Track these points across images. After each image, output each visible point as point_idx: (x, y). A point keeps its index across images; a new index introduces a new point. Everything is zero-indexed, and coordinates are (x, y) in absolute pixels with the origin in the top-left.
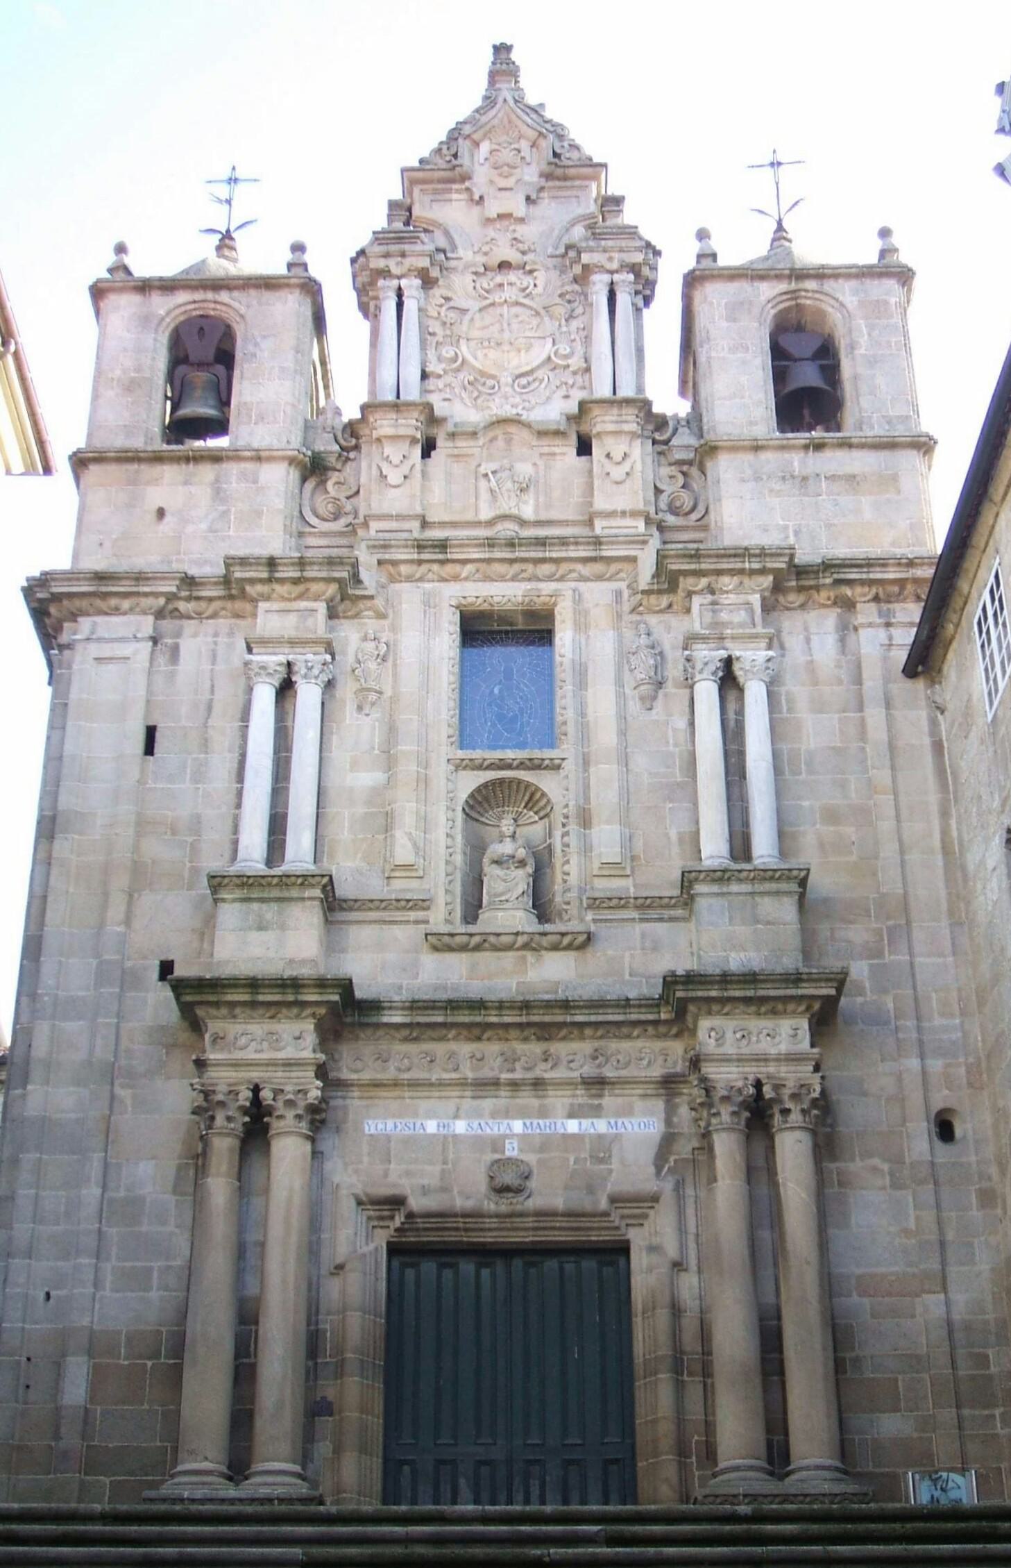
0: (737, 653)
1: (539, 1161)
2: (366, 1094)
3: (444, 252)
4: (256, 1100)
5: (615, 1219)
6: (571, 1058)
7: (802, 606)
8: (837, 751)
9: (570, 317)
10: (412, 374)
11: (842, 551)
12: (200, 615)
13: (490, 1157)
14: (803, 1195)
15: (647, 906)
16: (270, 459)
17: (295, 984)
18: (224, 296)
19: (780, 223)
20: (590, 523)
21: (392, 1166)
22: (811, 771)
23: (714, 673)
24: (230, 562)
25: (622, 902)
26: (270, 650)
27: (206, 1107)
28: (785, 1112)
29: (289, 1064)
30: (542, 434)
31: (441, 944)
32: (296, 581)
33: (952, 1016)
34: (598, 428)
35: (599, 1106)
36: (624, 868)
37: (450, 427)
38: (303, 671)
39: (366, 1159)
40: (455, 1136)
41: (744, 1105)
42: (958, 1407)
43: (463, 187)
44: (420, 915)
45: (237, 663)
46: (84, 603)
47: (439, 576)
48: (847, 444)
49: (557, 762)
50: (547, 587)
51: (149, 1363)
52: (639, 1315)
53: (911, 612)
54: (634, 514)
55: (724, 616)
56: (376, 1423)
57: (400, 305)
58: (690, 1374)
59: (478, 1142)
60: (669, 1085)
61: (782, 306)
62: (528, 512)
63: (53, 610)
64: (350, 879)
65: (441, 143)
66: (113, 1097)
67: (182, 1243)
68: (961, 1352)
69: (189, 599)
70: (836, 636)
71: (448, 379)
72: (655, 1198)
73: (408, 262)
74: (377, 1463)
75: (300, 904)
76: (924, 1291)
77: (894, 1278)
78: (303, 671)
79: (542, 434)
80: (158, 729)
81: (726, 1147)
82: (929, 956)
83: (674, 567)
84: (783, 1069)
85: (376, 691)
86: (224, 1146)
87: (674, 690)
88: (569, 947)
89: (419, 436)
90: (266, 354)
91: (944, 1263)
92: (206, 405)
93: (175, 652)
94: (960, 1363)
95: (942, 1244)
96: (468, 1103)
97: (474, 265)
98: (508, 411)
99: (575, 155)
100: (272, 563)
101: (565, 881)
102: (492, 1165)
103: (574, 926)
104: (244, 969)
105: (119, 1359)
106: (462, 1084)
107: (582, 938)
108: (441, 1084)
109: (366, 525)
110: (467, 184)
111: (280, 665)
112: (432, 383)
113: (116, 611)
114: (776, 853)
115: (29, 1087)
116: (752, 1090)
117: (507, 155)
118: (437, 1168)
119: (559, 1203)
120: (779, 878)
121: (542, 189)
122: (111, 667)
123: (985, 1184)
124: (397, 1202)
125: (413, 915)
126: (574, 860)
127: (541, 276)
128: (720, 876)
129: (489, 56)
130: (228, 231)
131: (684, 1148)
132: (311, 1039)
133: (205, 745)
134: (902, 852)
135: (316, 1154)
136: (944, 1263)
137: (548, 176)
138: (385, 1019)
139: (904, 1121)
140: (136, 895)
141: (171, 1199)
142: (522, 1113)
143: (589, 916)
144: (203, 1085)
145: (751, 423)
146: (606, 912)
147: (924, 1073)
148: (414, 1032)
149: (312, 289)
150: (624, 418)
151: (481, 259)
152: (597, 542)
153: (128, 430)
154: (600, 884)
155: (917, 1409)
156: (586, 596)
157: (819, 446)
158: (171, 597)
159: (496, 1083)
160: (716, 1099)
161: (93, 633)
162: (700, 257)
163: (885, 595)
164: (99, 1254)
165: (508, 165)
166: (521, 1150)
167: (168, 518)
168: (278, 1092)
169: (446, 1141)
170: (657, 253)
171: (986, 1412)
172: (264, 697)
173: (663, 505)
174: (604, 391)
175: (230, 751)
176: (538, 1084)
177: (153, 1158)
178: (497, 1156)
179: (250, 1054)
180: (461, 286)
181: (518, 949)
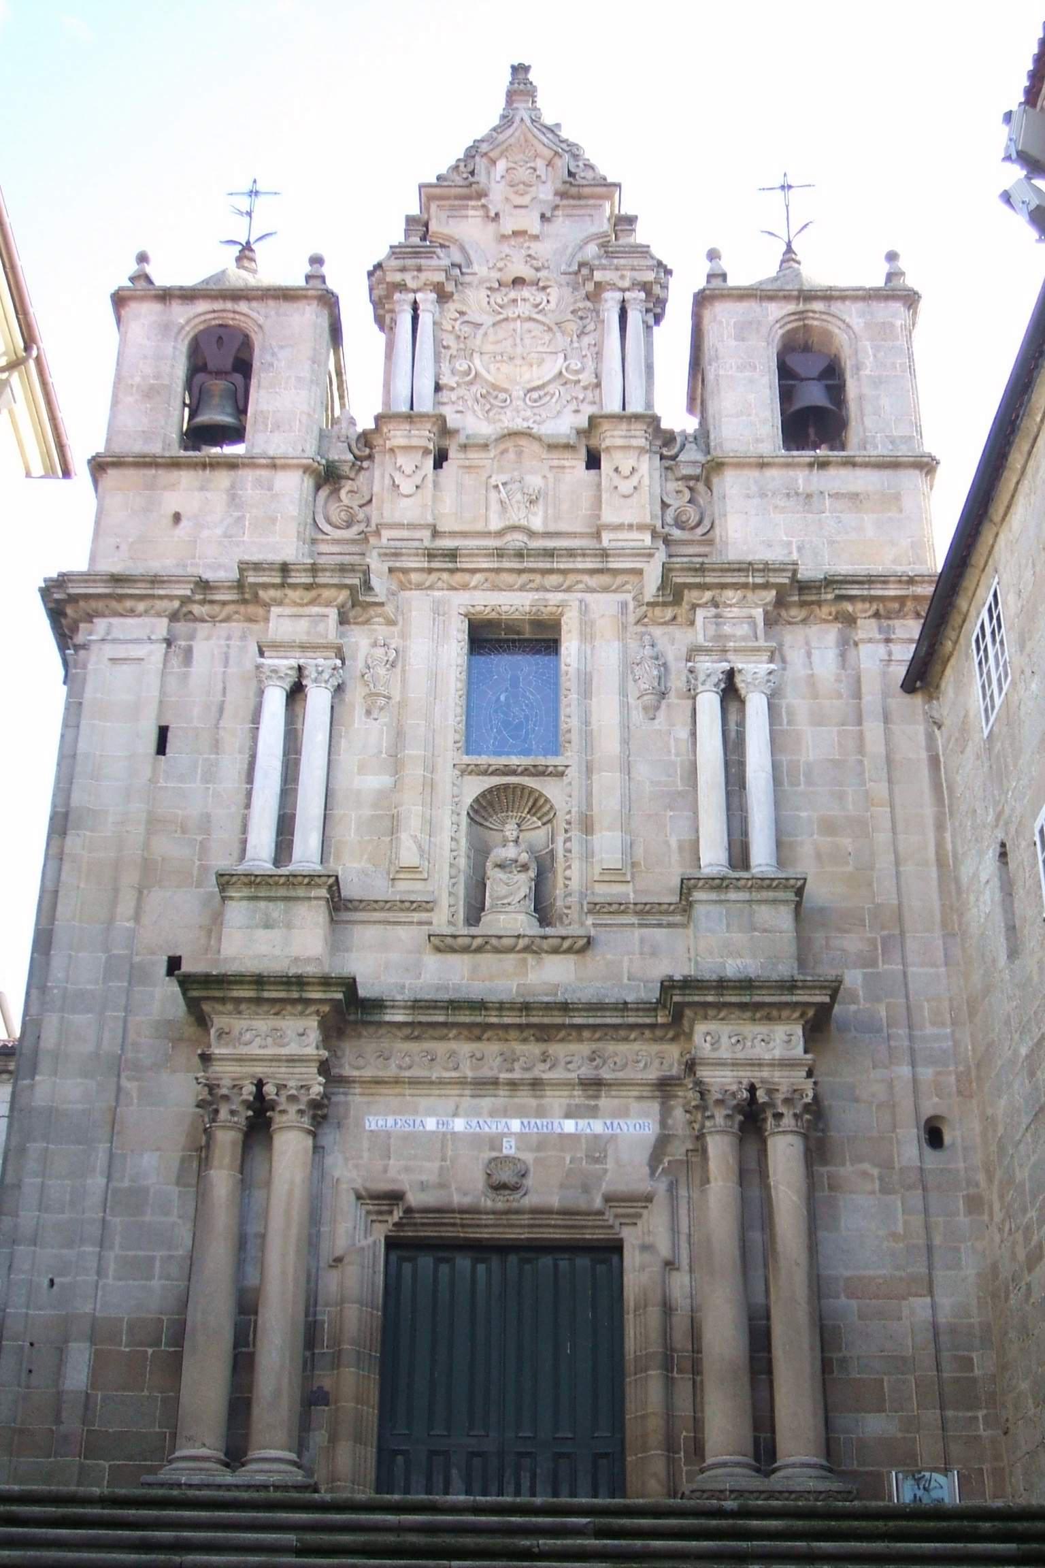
1: (536, 1160)
2: (367, 1091)
3: (460, 267)
4: (260, 1094)
5: (609, 1217)
6: (569, 1059)
7: (804, 621)
8: (837, 764)
9: (582, 334)
10: (425, 386)
11: (843, 568)
12: (213, 618)
13: (488, 1155)
14: (795, 1198)
15: (647, 912)
16: (285, 467)
17: (299, 982)
18: (243, 307)
19: (789, 244)
20: (597, 535)
21: (392, 1162)
22: (809, 783)
23: (716, 685)
24: (244, 567)
25: (622, 907)
27: (210, 1101)
29: (292, 1060)
30: (552, 447)
31: (444, 945)
32: (308, 587)
33: (943, 1024)
34: (607, 443)
36: (625, 874)
37: (462, 439)
38: (314, 675)
39: (366, 1155)
40: (454, 1134)
41: (738, 1108)
42: (942, 1408)
43: (480, 203)
44: (424, 916)
45: (249, 666)
46: (100, 605)
48: (850, 463)
49: (560, 769)
50: (555, 598)
51: (150, 1351)
52: (631, 1312)
53: (910, 628)
54: (641, 527)
55: (727, 629)
56: (371, 1413)
57: (415, 319)
58: (680, 1371)
59: (476, 1140)
60: (664, 1087)
61: (789, 326)
62: (537, 524)
63: (69, 611)
64: (355, 880)
65: (459, 160)
67: (184, 1234)
68: (945, 1355)
69: (203, 602)
70: (837, 651)
71: (461, 391)
72: (649, 1199)
73: (424, 276)
74: (371, 1452)
75: (306, 904)
76: (910, 1294)
77: (881, 1281)
79: (552, 447)
80: (170, 729)
81: (720, 1149)
83: (679, 580)
84: (777, 1074)
86: (227, 1139)
88: (569, 951)
89: (431, 447)
90: (283, 364)
91: (930, 1267)
93: (188, 654)
94: (945, 1365)
95: (930, 1248)
96: (467, 1102)
97: (489, 280)
98: (519, 424)
99: (589, 174)
100: (285, 568)
101: (566, 886)
102: (490, 1162)
103: (574, 930)
104: (251, 966)
106: (462, 1082)
107: (582, 942)
108: (441, 1083)
109: (377, 533)
110: (483, 201)
112: (445, 395)
113: (132, 613)
115: (37, 1078)
116: (745, 1094)
117: (523, 174)
118: (437, 1164)
119: (554, 1201)
120: (777, 887)
121: (556, 207)
122: (125, 668)
123: (972, 1191)
124: (395, 1197)
125: (416, 916)
126: (576, 865)
127: (554, 293)
128: (719, 884)
129: (508, 77)
130: (248, 243)
131: (678, 1150)
132: (314, 1035)
133: (216, 746)
134: (897, 863)
135: (317, 1149)
136: (930, 1267)
137: (563, 195)
138: (387, 1018)
139: (894, 1127)
140: (145, 892)
141: (174, 1191)
142: (520, 1113)
143: (590, 921)
145: (757, 441)
146: (607, 917)
147: (915, 1080)
148: (415, 1031)
149: (329, 301)
150: (633, 433)
151: (496, 275)
152: (604, 554)
153: (147, 436)
154: (601, 889)
155: (902, 1410)
156: (593, 606)
157: (823, 465)
158: (185, 600)
159: (495, 1083)
160: (711, 1102)
161: (108, 634)
162: (710, 277)
163: (886, 611)
164: (102, 1243)
165: (524, 183)
166: (518, 1148)
167: (184, 523)
169: (445, 1138)
170: (668, 272)
171: (970, 1414)
172: (275, 700)
173: (669, 519)
174: (613, 405)
176: (536, 1085)
177: (158, 1149)
178: (494, 1154)
179: (254, 1050)
180: (475, 300)
181: (519, 952)
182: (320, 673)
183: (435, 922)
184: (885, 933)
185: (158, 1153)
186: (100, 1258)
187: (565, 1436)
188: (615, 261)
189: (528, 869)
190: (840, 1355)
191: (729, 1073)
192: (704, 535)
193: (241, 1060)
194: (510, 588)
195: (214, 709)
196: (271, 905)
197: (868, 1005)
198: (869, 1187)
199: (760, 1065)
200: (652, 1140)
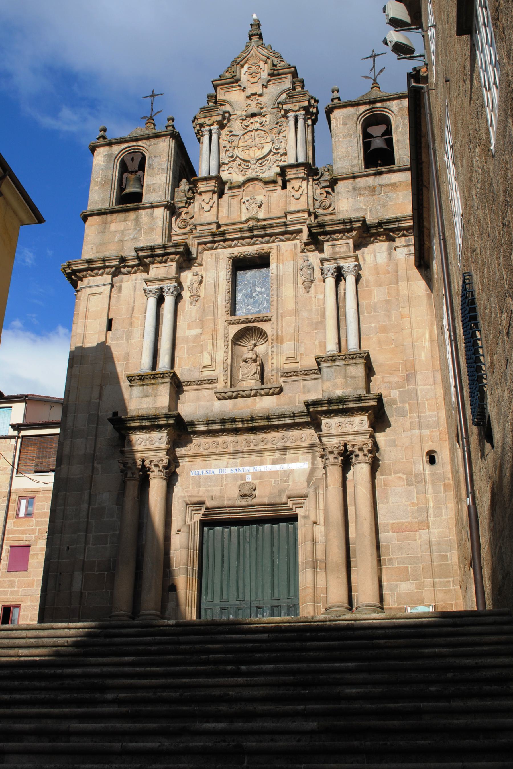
0: (341, 265)
2: (191, 460)
5: (290, 504)
6: (273, 439)
8: (387, 302)
10: (214, 164)
11: (390, 215)
12: (129, 273)
13: (240, 482)
15: (305, 373)
18: (140, 143)
19: (375, 80)
20: (286, 217)
21: (201, 489)
22: (375, 311)
23: (332, 274)
24: (138, 250)
25: (295, 373)
26: (154, 283)
28: (357, 456)
30: (266, 183)
35: (285, 459)
36: (296, 359)
38: (167, 290)
39: (191, 487)
40: (226, 475)
41: (340, 454)
43: (237, 84)
44: (214, 385)
47: (223, 246)
49: (269, 317)
51: (106, 573)
55: (337, 249)
58: (320, 569)
59: (235, 477)
62: (261, 216)
64: (186, 373)
65: (228, 68)
66: (93, 466)
68: (435, 555)
70: (387, 253)
75: (162, 385)
77: (407, 524)
78: (167, 290)
79: (266, 183)
80: (113, 320)
82: (424, 385)
83: (315, 231)
84: (357, 438)
85: (197, 296)
87: (318, 283)
88: (273, 394)
89: (216, 189)
90: (156, 164)
92: (136, 188)
94: (435, 559)
100: (152, 248)
101: (272, 366)
102: (240, 485)
105: (94, 571)
106: (228, 453)
107: (278, 390)
108: (220, 454)
110: (239, 83)
111: (157, 289)
113: (97, 274)
114: (338, 350)
115: (62, 466)
116: (342, 448)
117: (254, 69)
118: (219, 488)
119: (266, 500)
120: (356, 357)
121: (269, 81)
122: (96, 297)
124: (202, 503)
125: (211, 386)
126: (275, 357)
128: (332, 359)
133: (131, 324)
134: (413, 342)
137: (271, 75)
138: (197, 429)
140: (104, 387)
142: (253, 464)
143: (282, 380)
144: (122, 461)
145: (353, 167)
146: (289, 378)
147: (421, 435)
150: (299, 171)
151: (244, 113)
153: (103, 202)
154: (287, 366)
155: (417, 579)
156: (283, 247)
157: (380, 173)
161: (88, 284)
164: (87, 531)
165: (255, 73)
166: (252, 479)
168: (151, 462)
169: (222, 477)
171: (447, 580)
173: (317, 206)
175: (141, 326)
176: (260, 451)
177: (109, 491)
178: (243, 482)
180: (236, 126)
181: (252, 396)
182: (169, 289)
183: (218, 387)
184: (407, 373)
185: (109, 493)
186: (86, 536)
187: (459, 619)
188: (292, 99)
189: (256, 362)
190: (390, 557)
191: (335, 439)
192: (333, 210)
193: (202, 455)
194: (249, 244)
195: (131, 309)
196: (149, 387)
197: (401, 405)
198: (402, 484)
199: (349, 435)
200: (308, 470)
